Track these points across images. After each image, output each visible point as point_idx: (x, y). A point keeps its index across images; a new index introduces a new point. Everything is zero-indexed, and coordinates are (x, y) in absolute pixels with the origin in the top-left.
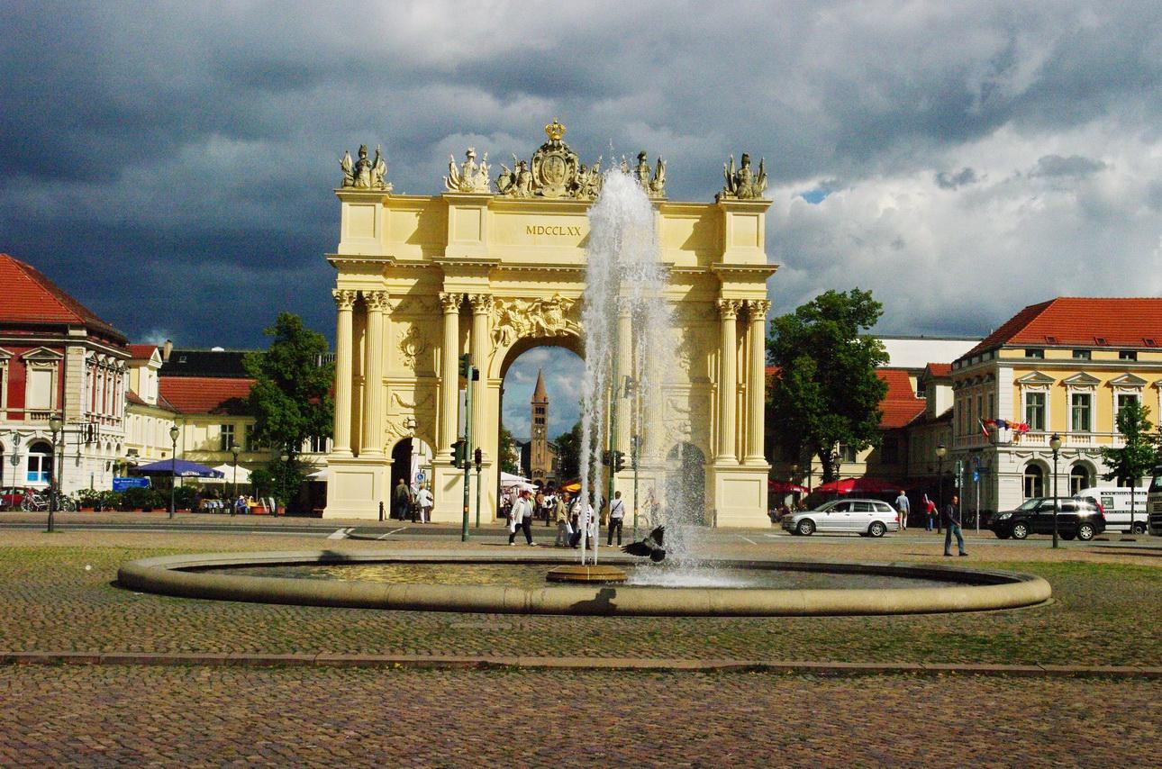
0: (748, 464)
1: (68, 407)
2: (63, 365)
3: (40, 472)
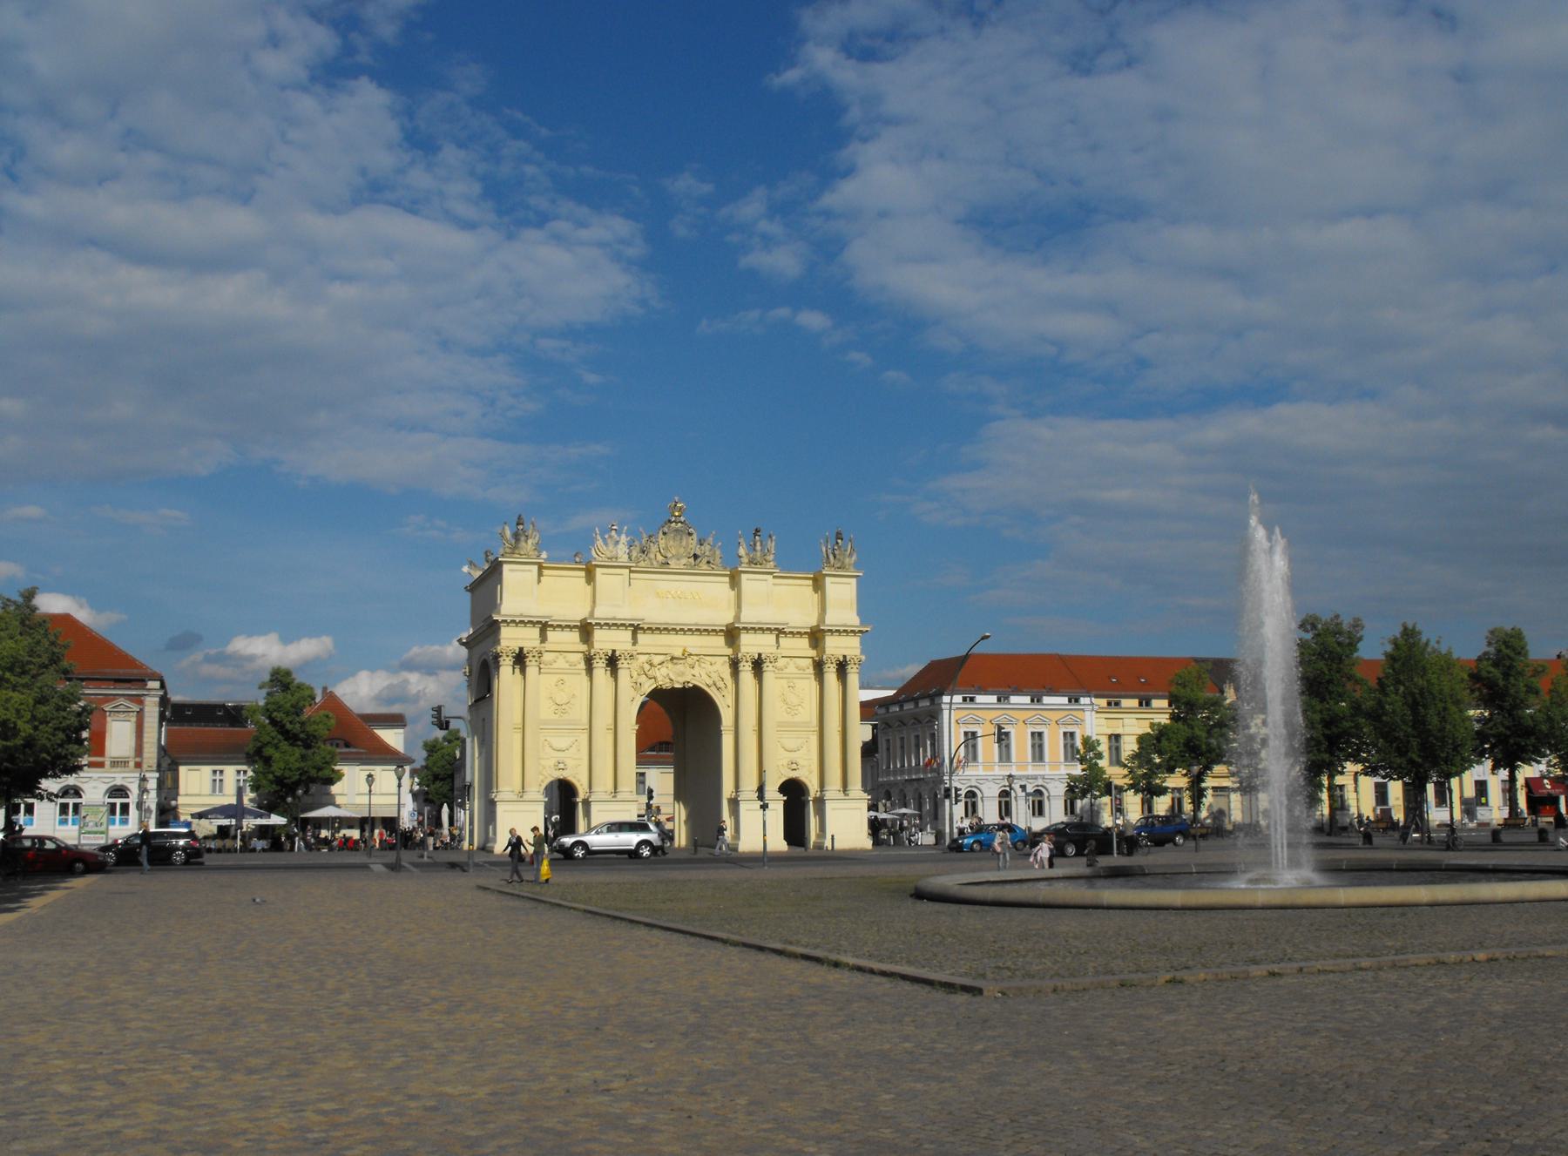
0: (619, 797)
2: (140, 715)
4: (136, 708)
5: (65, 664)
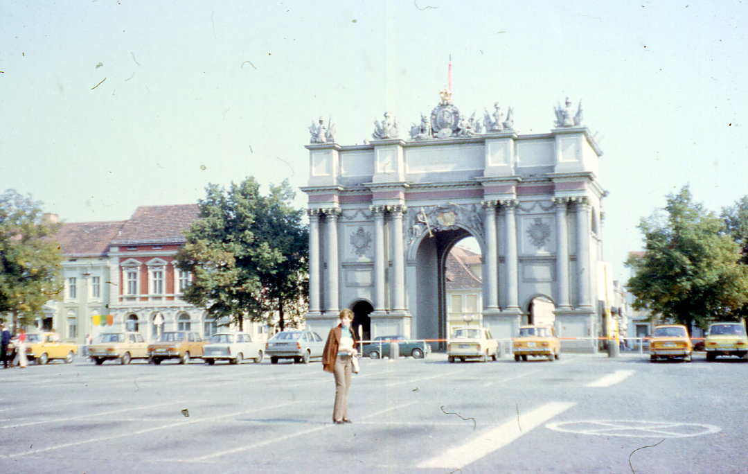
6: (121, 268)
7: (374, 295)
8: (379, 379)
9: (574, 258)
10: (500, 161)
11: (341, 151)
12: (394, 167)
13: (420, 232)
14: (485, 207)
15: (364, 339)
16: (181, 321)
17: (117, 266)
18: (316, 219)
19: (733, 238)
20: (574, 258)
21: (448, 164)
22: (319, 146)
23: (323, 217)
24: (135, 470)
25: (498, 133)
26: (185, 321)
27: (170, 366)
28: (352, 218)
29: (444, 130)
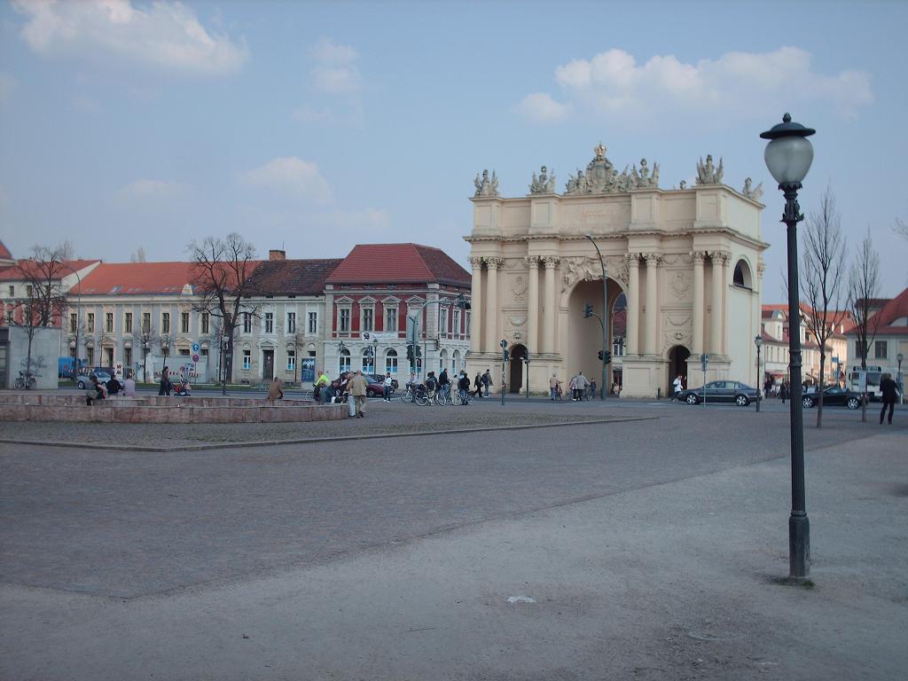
1: (428, 330)
3: (368, 367)
4: (422, 300)
5: (541, 173)
6: (335, 304)
7: (691, 339)
8: (798, 531)
9: (708, 309)
10: (647, 212)
11: (503, 202)
12: (549, 217)
13: (573, 280)
14: (629, 259)
15: (352, 330)
16: (389, 357)
17: (332, 302)
18: (479, 267)
19: (44, 363)
20: (708, 309)
21: (599, 216)
22: (484, 193)
23: (484, 266)
24: (344, 679)
25: (639, 184)
26: (392, 357)
27: (380, 280)
28: (512, 267)
29: (600, 180)
